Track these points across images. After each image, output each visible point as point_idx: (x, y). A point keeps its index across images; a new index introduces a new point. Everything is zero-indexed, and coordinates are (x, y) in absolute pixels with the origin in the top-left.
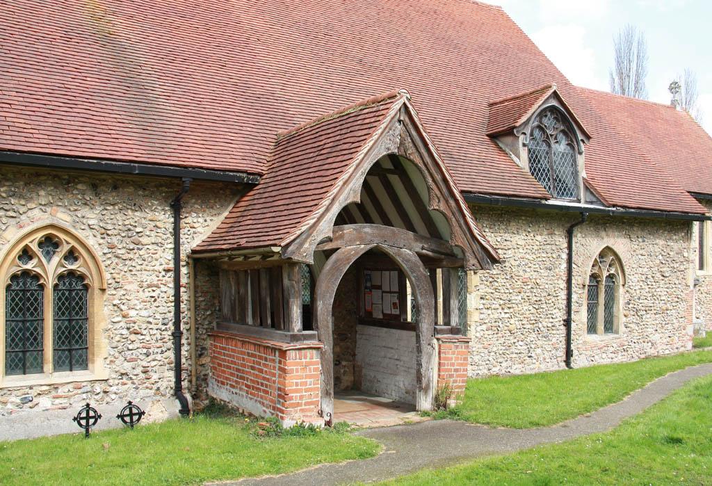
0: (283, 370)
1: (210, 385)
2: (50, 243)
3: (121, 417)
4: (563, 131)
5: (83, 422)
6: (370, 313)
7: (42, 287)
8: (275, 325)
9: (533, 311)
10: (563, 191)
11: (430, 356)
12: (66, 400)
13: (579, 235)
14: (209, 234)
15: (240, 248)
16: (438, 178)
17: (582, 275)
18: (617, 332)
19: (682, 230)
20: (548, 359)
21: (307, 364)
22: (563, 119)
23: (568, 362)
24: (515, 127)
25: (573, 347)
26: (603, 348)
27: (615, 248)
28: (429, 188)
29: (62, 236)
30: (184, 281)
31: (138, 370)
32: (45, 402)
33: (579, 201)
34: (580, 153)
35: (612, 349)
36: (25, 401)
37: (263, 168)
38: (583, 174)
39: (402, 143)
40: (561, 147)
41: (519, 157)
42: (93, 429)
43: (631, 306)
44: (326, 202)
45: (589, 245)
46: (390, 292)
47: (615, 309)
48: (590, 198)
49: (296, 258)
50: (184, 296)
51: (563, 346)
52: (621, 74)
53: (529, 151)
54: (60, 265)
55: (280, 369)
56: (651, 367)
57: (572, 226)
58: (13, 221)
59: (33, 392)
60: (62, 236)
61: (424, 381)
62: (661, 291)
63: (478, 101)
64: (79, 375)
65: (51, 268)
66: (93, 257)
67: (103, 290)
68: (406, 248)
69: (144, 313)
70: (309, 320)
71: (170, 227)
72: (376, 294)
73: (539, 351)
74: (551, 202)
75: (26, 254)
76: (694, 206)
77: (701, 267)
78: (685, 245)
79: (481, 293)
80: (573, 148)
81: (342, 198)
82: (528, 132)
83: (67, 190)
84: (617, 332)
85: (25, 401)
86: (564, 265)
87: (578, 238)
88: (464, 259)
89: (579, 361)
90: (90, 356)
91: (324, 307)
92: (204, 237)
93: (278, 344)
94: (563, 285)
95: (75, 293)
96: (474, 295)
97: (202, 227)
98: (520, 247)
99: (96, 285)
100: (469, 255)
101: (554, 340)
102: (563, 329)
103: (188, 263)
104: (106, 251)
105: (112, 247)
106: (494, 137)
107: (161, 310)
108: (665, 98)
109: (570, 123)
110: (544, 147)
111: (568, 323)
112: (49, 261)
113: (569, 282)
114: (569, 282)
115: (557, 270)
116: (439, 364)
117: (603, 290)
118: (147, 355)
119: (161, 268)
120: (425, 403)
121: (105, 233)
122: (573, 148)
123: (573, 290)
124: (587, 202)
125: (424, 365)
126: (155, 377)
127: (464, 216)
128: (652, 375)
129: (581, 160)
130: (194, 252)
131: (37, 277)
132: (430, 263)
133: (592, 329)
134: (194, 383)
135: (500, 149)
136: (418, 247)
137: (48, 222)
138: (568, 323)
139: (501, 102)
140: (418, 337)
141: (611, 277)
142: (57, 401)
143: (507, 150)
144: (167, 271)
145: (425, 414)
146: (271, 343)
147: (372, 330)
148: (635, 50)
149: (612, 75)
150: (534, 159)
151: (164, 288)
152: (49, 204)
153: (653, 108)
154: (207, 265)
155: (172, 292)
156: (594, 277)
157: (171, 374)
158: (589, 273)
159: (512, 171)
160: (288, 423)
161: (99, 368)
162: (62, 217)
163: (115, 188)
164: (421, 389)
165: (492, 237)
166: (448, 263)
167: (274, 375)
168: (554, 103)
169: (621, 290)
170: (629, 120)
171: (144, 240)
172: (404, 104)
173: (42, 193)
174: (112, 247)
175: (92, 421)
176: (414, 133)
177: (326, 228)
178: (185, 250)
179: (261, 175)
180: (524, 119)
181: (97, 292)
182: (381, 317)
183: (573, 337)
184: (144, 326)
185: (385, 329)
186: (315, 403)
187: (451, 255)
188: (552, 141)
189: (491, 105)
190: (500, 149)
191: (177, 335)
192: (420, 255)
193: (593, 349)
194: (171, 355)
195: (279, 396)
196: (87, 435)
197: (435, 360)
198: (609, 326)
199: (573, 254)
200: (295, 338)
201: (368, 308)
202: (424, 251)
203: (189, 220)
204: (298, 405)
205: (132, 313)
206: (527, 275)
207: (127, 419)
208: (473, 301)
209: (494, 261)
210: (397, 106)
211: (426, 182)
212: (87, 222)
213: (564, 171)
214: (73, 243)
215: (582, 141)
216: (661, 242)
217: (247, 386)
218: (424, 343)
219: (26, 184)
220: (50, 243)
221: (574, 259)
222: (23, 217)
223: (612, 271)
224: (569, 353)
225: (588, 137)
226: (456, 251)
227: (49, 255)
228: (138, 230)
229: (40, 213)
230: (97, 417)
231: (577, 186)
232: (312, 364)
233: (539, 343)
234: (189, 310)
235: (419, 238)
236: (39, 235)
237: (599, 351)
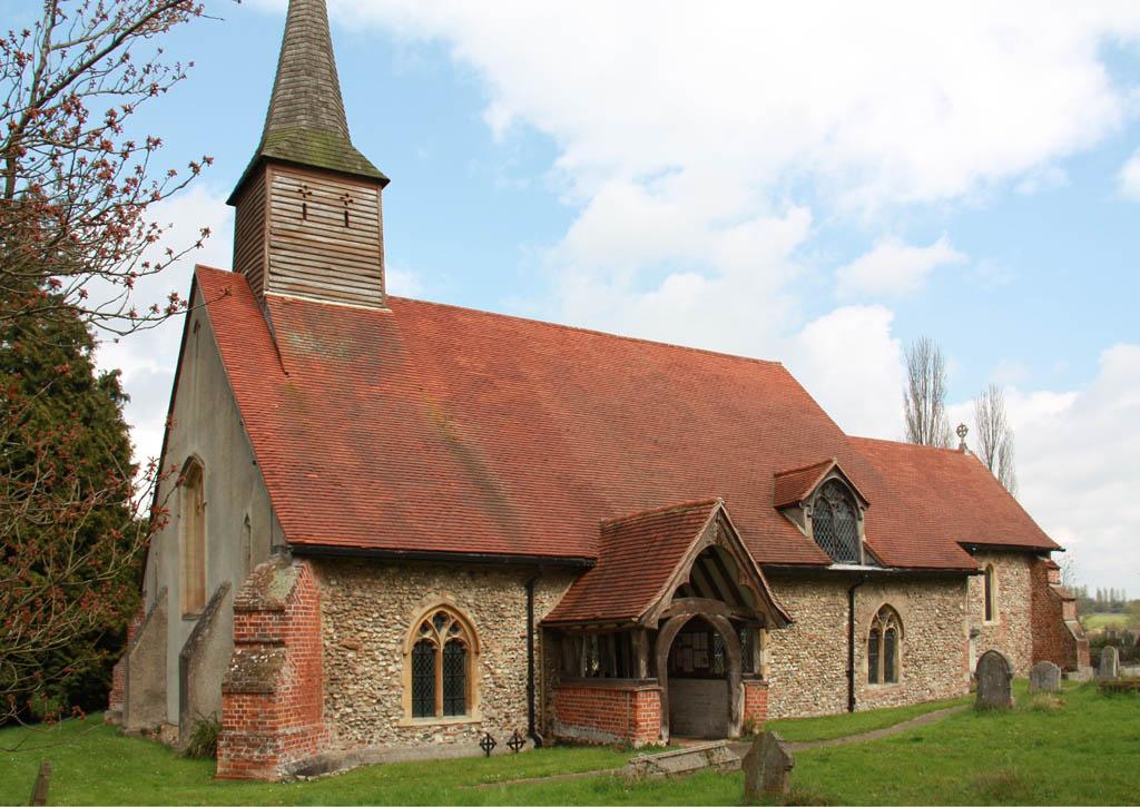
1: (556, 727)
3: (510, 744)
4: (844, 501)
5: (514, 746)
6: (682, 668)
7: (434, 651)
9: (818, 664)
11: (739, 696)
12: (452, 738)
13: (860, 595)
14: (554, 607)
15: (596, 619)
16: (745, 561)
17: (864, 629)
18: (897, 681)
19: (957, 584)
21: (652, 701)
22: (843, 492)
23: (851, 708)
24: (800, 501)
25: (855, 696)
27: (893, 605)
28: (739, 570)
29: (449, 612)
31: (502, 716)
33: (859, 564)
34: (860, 519)
35: (891, 697)
36: (426, 736)
37: (595, 553)
38: (863, 538)
40: (841, 516)
41: (804, 527)
42: (492, 752)
43: (909, 657)
44: (667, 585)
45: (869, 603)
46: (700, 650)
47: (894, 660)
48: (870, 560)
49: (646, 625)
51: (846, 695)
52: (915, 396)
53: (813, 521)
54: (448, 635)
55: (631, 706)
56: (925, 707)
57: (853, 588)
58: (417, 602)
59: (431, 731)
60: (449, 612)
61: (734, 716)
62: (938, 641)
63: (762, 471)
64: (460, 719)
65: (443, 635)
67: (477, 653)
68: (721, 616)
69: (507, 671)
70: (652, 670)
71: (525, 603)
72: (687, 652)
73: (824, 699)
75: (425, 627)
76: (964, 560)
77: (988, 618)
78: (960, 598)
79: (773, 649)
80: (853, 515)
81: (677, 581)
82: (812, 504)
83: (453, 577)
84: (897, 681)
85: (426, 736)
86: (846, 623)
87: (859, 597)
89: (860, 706)
90: (468, 705)
91: (662, 660)
92: (550, 610)
93: (630, 688)
94: (845, 640)
95: (458, 656)
96: (766, 651)
97: (548, 603)
98: (809, 610)
99: (473, 649)
101: (838, 690)
103: (538, 632)
104: (480, 623)
105: (483, 620)
106: (781, 509)
108: (955, 444)
109: (848, 491)
110: (827, 516)
111: (850, 674)
112: (439, 631)
115: (840, 627)
116: (746, 702)
118: (509, 703)
119: (518, 636)
120: (735, 732)
121: (479, 609)
122: (853, 515)
124: (867, 564)
125: (734, 703)
126: (514, 721)
127: (765, 588)
128: (921, 712)
129: (861, 526)
130: (542, 622)
133: (873, 679)
134: (543, 726)
135: (787, 520)
136: (728, 613)
137: (442, 602)
138: (850, 674)
139: (786, 473)
140: (729, 683)
141: (890, 631)
142: (447, 738)
143: (793, 521)
144: (522, 637)
145: (735, 739)
147: (684, 681)
148: (930, 365)
149: (906, 396)
150: (816, 525)
151: (521, 652)
152: (442, 588)
153: (944, 453)
155: (526, 654)
156: (875, 632)
157: (525, 719)
158: (869, 628)
159: (800, 539)
160: (638, 744)
161: (475, 714)
162: (450, 599)
163: (486, 574)
165: (783, 601)
166: (753, 622)
167: (625, 711)
168: (835, 476)
169: (900, 643)
170: (915, 470)
172: (721, 509)
173: (437, 580)
174: (483, 620)
175: (519, 745)
176: (727, 529)
177: (666, 603)
178: (537, 620)
179: (595, 559)
181: (473, 655)
182: (691, 670)
183: (855, 686)
184: (506, 681)
185: (696, 681)
186: (657, 730)
187: (754, 619)
188: (834, 511)
189: (777, 476)
190: (787, 520)
191: (530, 689)
192: (731, 620)
193: (872, 695)
194: (525, 704)
195: (630, 725)
196: (488, 755)
197: (742, 699)
198: (890, 677)
199: (855, 611)
200: (643, 683)
201: (679, 664)
202: (734, 617)
203: (539, 597)
204: (646, 731)
205: (499, 671)
206: (813, 633)
207: (514, 746)
209: (130, 286)
210: (715, 510)
211: (736, 565)
212: (467, 601)
213: (845, 537)
214: (457, 618)
215: (862, 508)
216: (937, 597)
217: (599, 723)
218: (733, 686)
219: (427, 574)
220: (440, 618)
221: (855, 616)
222: (424, 599)
223: (892, 626)
224: (852, 701)
225: (867, 504)
226: (757, 615)
227: (439, 627)
228: (503, 606)
229: (433, 597)
230: (494, 744)
231: (858, 550)
232: (654, 701)
234: (539, 668)
235: (729, 606)
236: (434, 612)
237: (879, 699)
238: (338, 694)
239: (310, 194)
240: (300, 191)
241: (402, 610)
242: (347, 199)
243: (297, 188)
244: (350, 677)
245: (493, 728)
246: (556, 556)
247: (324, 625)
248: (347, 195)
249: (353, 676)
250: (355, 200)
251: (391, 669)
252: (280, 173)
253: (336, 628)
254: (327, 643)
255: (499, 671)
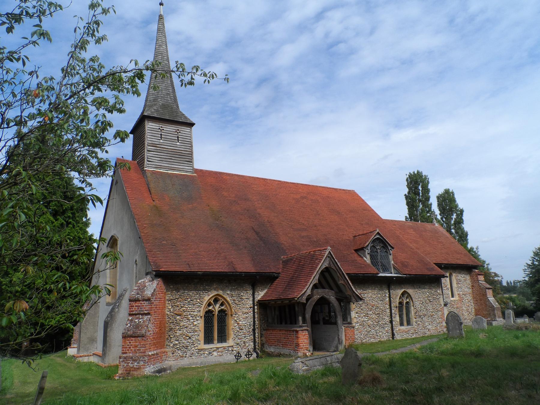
0: (298, 337)
2: (216, 301)
7: (213, 315)
8: (291, 323)
10: (385, 270)
17: (396, 302)
20: (385, 336)
21: (305, 335)
23: (393, 338)
26: (407, 332)
28: (338, 277)
30: (256, 311)
31: (242, 343)
32: (215, 354)
33: (391, 273)
36: (210, 353)
39: (329, 263)
50: (256, 316)
51: (390, 331)
54: (219, 307)
58: (207, 294)
62: (430, 307)
66: (229, 304)
68: (332, 297)
69: (244, 322)
70: (304, 321)
73: (381, 333)
74: (380, 275)
75: (209, 305)
85: (210, 353)
86: (388, 299)
88: (351, 299)
90: (227, 338)
91: (308, 316)
94: (388, 307)
98: (371, 296)
99: (230, 314)
100: (352, 297)
102: (390, 324)
105: (234, 300)
106: (356, 251)
107: (249, 321)
111: (391, 322)
113: (390, 305)
114: (390, 305)
117: (404, 308)
118: (245, 337)
123: (393, 308)
124: (395, 273)
126: (247, 345)
131: (213, 311)
132: (339, 300)
133: (402, 324)
135: (360, 256)
138: (391, 322)
141: (407, 303)
144: (250, 308)
146: (293, 329)
154: (263, 305)
155: (252, 315)
156: (400, 303)
157: (252, 344)
158: (398, 302)
164: (339, 343)
166: (346, 300)
168: (378, 236)
169: (412, 308)
171: (243, 297)
174: (234, 300)
180: (367, 244)
181: (230, 316)
187: (346, 298)
191: (254, 330)
193: (402, 332)
194: (252, 337)
200: (301, 327)
205: (240, 322)
208: (353, 314)
209: (361, 299)
210: (327, 253)
220: (216, 301)
224: (393, 335)
225: (393, 248)
233: (380, 330)
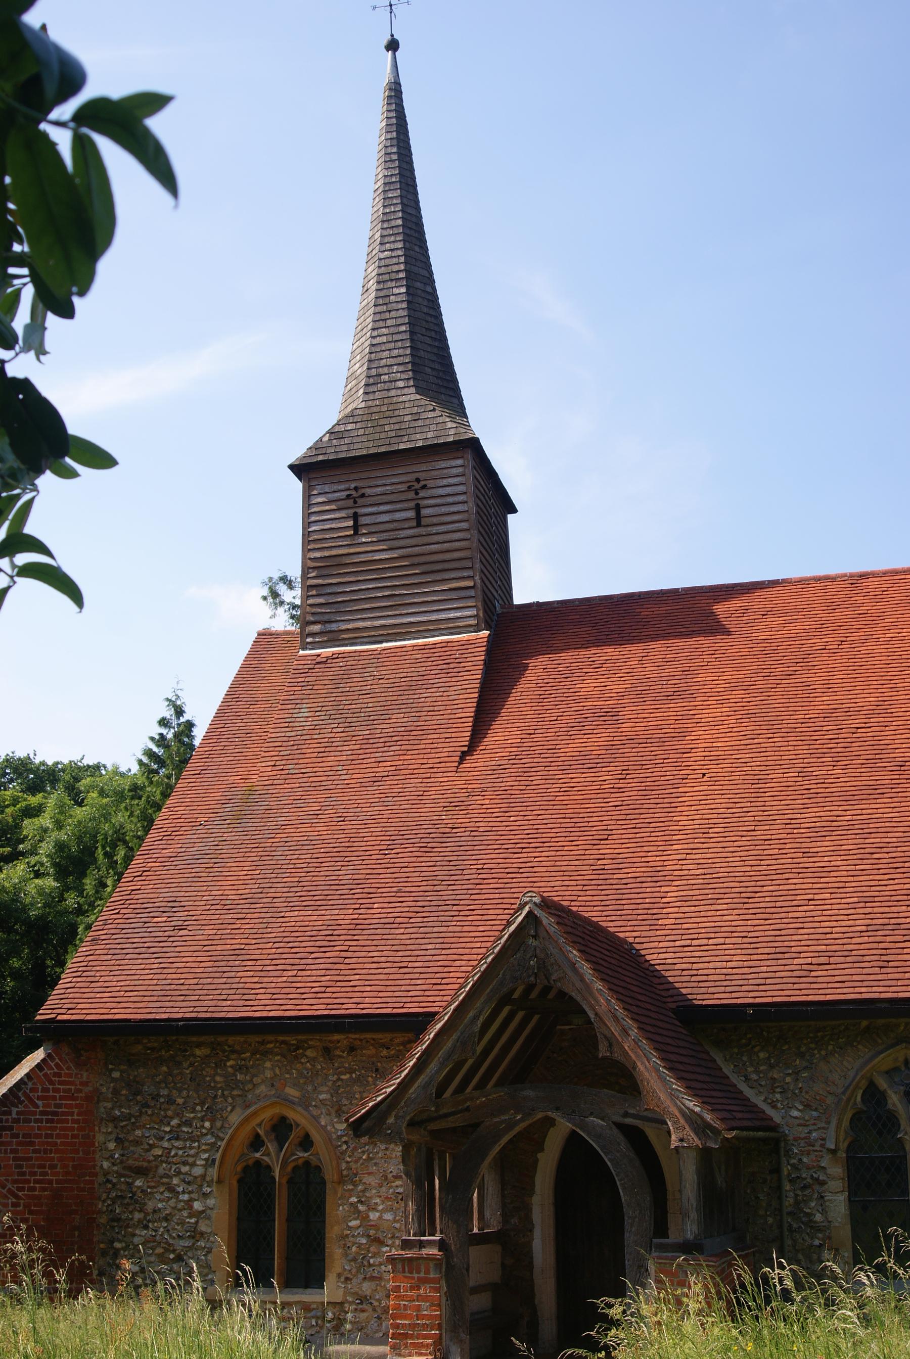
64: (309, 1296)
220: (281, 1128)
238: (120, 1241)
239: (363, 495)
240: (348, 496)
241: (211, 1113)
242: (417, 486)
243: (344, 494)
244: (137, 1216)
245: (365, 1315)
246: (182, 1019)
247: (100, 1138)
248: (418, 480)
249: (141, 1215)
250: (430, 484)
251: (197, 1205)
252: (321, 481)
253: (118, 1140)
254: (106, 1164)
255: (374, 1216)
